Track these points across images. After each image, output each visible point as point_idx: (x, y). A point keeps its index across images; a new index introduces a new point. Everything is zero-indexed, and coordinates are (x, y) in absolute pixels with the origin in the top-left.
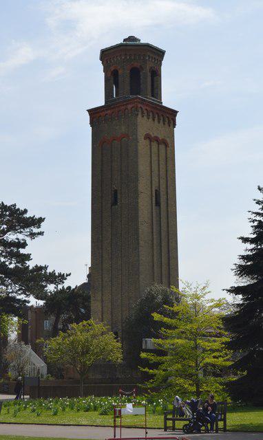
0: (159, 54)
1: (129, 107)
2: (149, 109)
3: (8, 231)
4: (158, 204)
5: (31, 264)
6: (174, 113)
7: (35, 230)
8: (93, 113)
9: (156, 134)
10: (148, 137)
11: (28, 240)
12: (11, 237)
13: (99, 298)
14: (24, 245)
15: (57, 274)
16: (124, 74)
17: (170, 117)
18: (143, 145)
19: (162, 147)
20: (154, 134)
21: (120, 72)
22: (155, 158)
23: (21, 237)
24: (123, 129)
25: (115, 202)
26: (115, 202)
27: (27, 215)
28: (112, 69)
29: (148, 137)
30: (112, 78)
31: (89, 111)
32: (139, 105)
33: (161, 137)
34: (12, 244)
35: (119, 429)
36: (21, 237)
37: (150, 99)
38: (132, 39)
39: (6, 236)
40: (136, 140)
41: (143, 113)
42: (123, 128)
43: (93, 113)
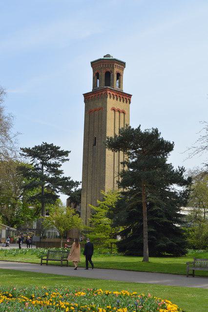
0: (123, 64)
1: (104, 92)
2: (114, 94)
3: (50, 158)
5: (61, 176)
6: (130, 96)
7: (66, 158)
8: (86, 96)
9: (118, 107)
10: (114, 109)
11: (61, 163)
12: (52, 161)
13: (85, 195)
14: (60, 166)
15: (75, 182)
16: (102, 75)
17: (127, 98)
18: (110, 114)
19: (122, 115)
21: (100, 74)
22: (117, 120)
23: (57, 161)
24: (100, 105)
25: (95, 144)
26: (95, 144)
27: (60, 150)
29: (114, 109)
30: (96, 76)
31: (84, 95)
35: (43, 261)
36: (57, 161)
37: (119, 90)
38: (108, 56)
39: (50, 160)
41: (110, 96)
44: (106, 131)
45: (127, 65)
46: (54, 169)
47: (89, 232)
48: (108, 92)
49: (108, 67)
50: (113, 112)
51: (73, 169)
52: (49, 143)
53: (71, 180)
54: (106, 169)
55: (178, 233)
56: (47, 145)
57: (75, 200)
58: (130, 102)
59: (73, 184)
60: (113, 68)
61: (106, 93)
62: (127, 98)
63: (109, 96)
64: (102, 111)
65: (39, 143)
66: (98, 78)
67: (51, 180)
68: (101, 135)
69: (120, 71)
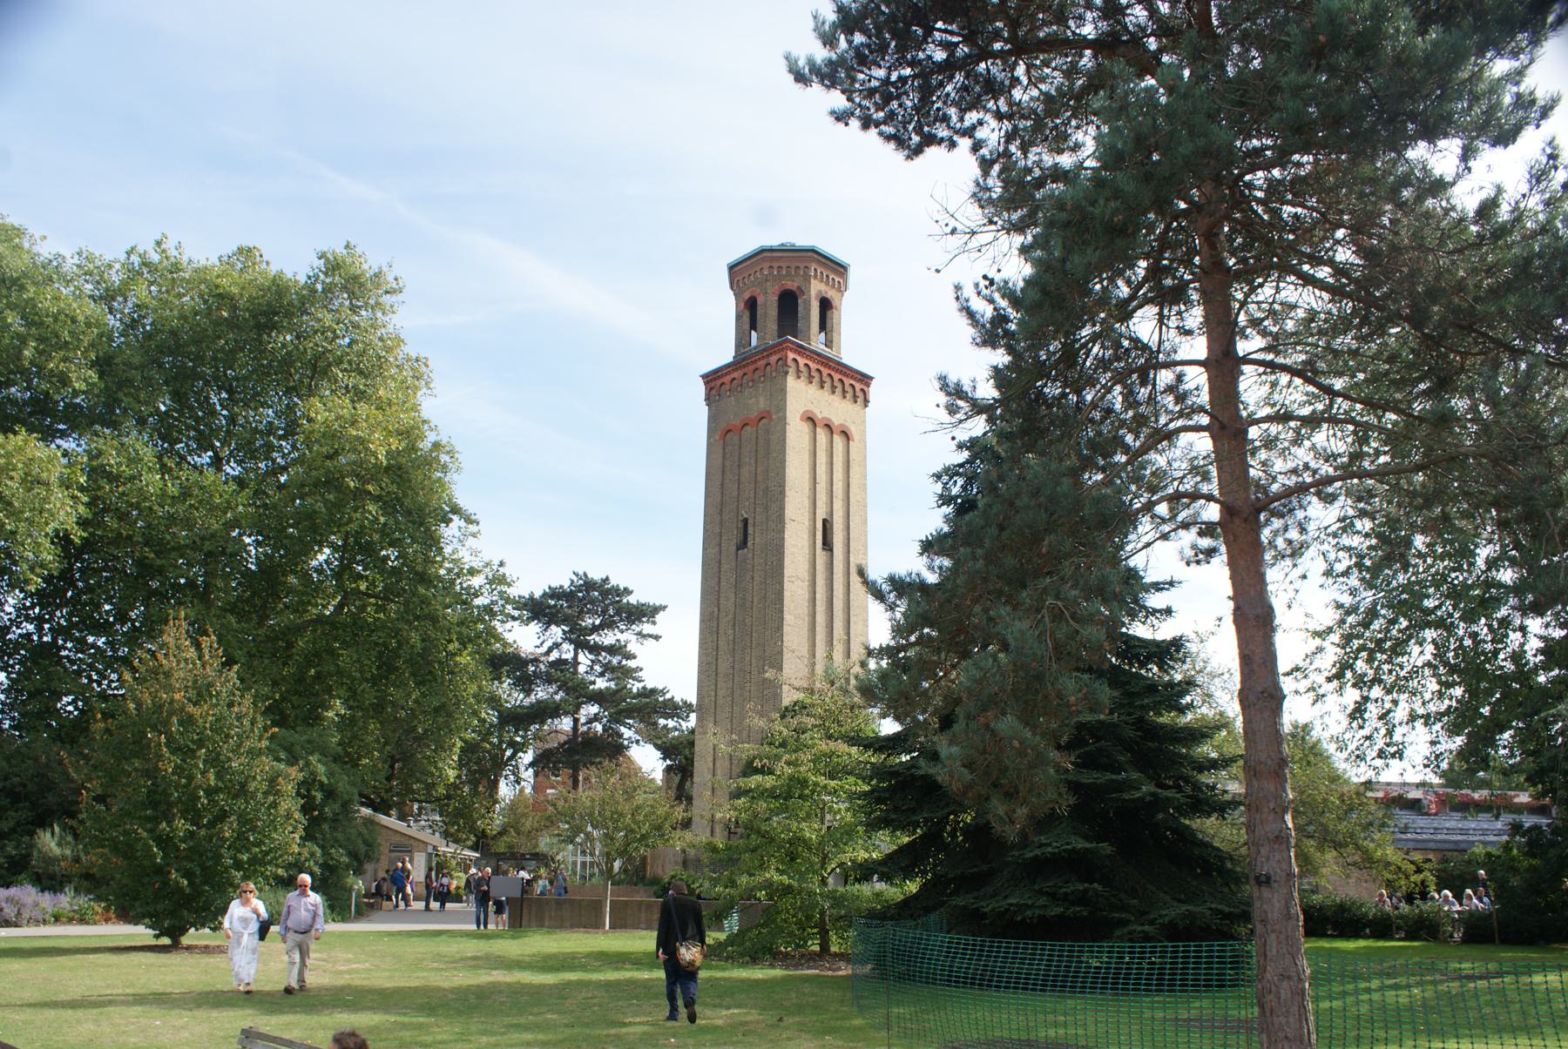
0: (840, 269)
1: (773, 359)
4: (827, 545)
8: (713, 380)
9: (825, 414)
10: (811, 420)
12: (608, 638)
17: (858, 386)
18: (797, 434)
19: (838, 441)
20: (821, 413)
24: (762, 403)
27: (632, 599)
28: (747, 296)
29: (811, 420)
30: (749, 311)
31: (703, 377)
32: (791, 355)
33: (836, 421)
34: (613, 650)
36: (623, 637)
40: (783, 421)
41: (798, 371)
42: (762, 400)
43: (713, 380)
44: (783, 493)
45: (853, 275)
46: (618, 664)
47: (810, 849)
48: (791, 355)
49: (788, 274)
50: (805, 428)
51: (669, 660)
52: (596, 575)
53: (668, 696)
54: (786, 628)
55: (1211, 867)
56: (589, 585)
57: (680, 755)
58: (866, 402)
59: (675, 709)
60: (807, 278)
61: (784, 359)
62: (855, 384)
63: (792, 370)
64: (769, 425)
65: (563, 579)
66: (753, 326)
67: (599, 697)
68: (766, 508)
69: (831, 293)
